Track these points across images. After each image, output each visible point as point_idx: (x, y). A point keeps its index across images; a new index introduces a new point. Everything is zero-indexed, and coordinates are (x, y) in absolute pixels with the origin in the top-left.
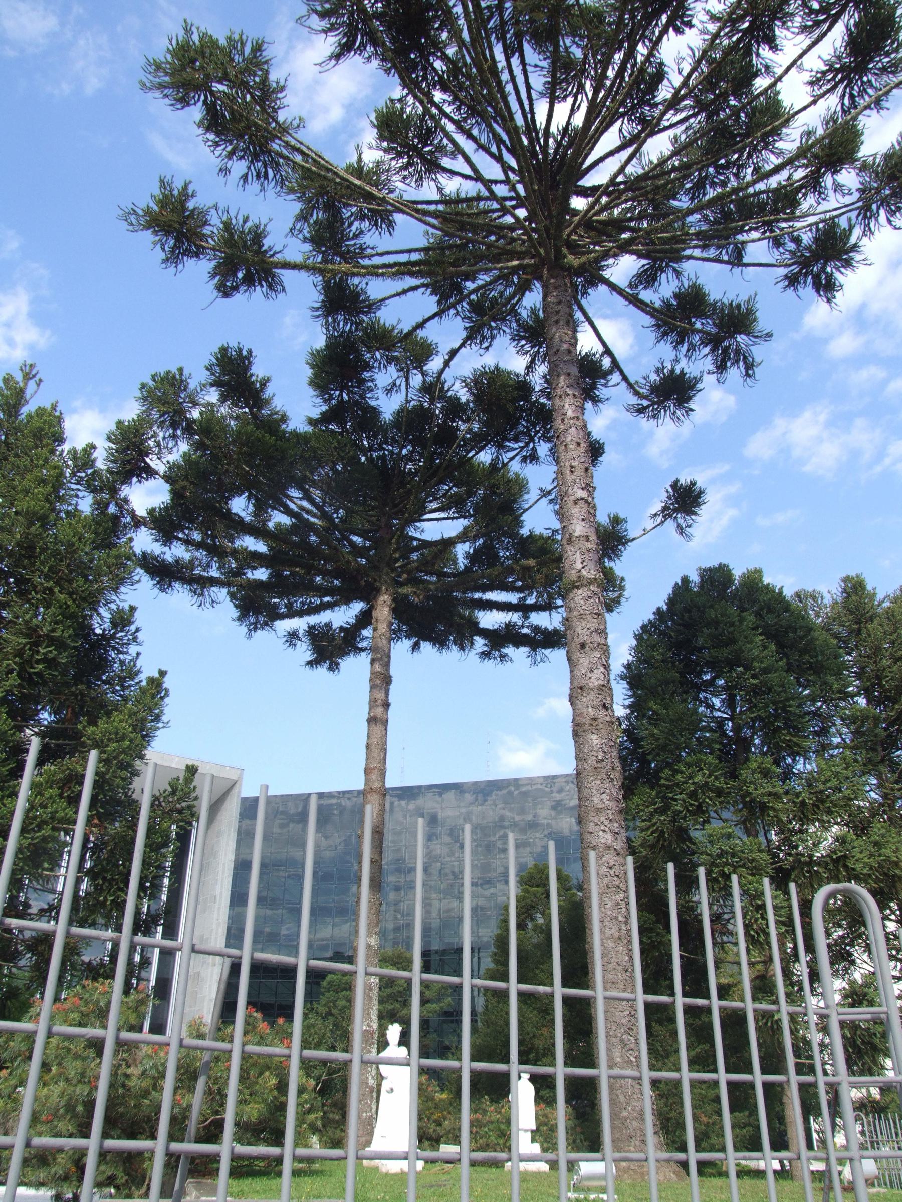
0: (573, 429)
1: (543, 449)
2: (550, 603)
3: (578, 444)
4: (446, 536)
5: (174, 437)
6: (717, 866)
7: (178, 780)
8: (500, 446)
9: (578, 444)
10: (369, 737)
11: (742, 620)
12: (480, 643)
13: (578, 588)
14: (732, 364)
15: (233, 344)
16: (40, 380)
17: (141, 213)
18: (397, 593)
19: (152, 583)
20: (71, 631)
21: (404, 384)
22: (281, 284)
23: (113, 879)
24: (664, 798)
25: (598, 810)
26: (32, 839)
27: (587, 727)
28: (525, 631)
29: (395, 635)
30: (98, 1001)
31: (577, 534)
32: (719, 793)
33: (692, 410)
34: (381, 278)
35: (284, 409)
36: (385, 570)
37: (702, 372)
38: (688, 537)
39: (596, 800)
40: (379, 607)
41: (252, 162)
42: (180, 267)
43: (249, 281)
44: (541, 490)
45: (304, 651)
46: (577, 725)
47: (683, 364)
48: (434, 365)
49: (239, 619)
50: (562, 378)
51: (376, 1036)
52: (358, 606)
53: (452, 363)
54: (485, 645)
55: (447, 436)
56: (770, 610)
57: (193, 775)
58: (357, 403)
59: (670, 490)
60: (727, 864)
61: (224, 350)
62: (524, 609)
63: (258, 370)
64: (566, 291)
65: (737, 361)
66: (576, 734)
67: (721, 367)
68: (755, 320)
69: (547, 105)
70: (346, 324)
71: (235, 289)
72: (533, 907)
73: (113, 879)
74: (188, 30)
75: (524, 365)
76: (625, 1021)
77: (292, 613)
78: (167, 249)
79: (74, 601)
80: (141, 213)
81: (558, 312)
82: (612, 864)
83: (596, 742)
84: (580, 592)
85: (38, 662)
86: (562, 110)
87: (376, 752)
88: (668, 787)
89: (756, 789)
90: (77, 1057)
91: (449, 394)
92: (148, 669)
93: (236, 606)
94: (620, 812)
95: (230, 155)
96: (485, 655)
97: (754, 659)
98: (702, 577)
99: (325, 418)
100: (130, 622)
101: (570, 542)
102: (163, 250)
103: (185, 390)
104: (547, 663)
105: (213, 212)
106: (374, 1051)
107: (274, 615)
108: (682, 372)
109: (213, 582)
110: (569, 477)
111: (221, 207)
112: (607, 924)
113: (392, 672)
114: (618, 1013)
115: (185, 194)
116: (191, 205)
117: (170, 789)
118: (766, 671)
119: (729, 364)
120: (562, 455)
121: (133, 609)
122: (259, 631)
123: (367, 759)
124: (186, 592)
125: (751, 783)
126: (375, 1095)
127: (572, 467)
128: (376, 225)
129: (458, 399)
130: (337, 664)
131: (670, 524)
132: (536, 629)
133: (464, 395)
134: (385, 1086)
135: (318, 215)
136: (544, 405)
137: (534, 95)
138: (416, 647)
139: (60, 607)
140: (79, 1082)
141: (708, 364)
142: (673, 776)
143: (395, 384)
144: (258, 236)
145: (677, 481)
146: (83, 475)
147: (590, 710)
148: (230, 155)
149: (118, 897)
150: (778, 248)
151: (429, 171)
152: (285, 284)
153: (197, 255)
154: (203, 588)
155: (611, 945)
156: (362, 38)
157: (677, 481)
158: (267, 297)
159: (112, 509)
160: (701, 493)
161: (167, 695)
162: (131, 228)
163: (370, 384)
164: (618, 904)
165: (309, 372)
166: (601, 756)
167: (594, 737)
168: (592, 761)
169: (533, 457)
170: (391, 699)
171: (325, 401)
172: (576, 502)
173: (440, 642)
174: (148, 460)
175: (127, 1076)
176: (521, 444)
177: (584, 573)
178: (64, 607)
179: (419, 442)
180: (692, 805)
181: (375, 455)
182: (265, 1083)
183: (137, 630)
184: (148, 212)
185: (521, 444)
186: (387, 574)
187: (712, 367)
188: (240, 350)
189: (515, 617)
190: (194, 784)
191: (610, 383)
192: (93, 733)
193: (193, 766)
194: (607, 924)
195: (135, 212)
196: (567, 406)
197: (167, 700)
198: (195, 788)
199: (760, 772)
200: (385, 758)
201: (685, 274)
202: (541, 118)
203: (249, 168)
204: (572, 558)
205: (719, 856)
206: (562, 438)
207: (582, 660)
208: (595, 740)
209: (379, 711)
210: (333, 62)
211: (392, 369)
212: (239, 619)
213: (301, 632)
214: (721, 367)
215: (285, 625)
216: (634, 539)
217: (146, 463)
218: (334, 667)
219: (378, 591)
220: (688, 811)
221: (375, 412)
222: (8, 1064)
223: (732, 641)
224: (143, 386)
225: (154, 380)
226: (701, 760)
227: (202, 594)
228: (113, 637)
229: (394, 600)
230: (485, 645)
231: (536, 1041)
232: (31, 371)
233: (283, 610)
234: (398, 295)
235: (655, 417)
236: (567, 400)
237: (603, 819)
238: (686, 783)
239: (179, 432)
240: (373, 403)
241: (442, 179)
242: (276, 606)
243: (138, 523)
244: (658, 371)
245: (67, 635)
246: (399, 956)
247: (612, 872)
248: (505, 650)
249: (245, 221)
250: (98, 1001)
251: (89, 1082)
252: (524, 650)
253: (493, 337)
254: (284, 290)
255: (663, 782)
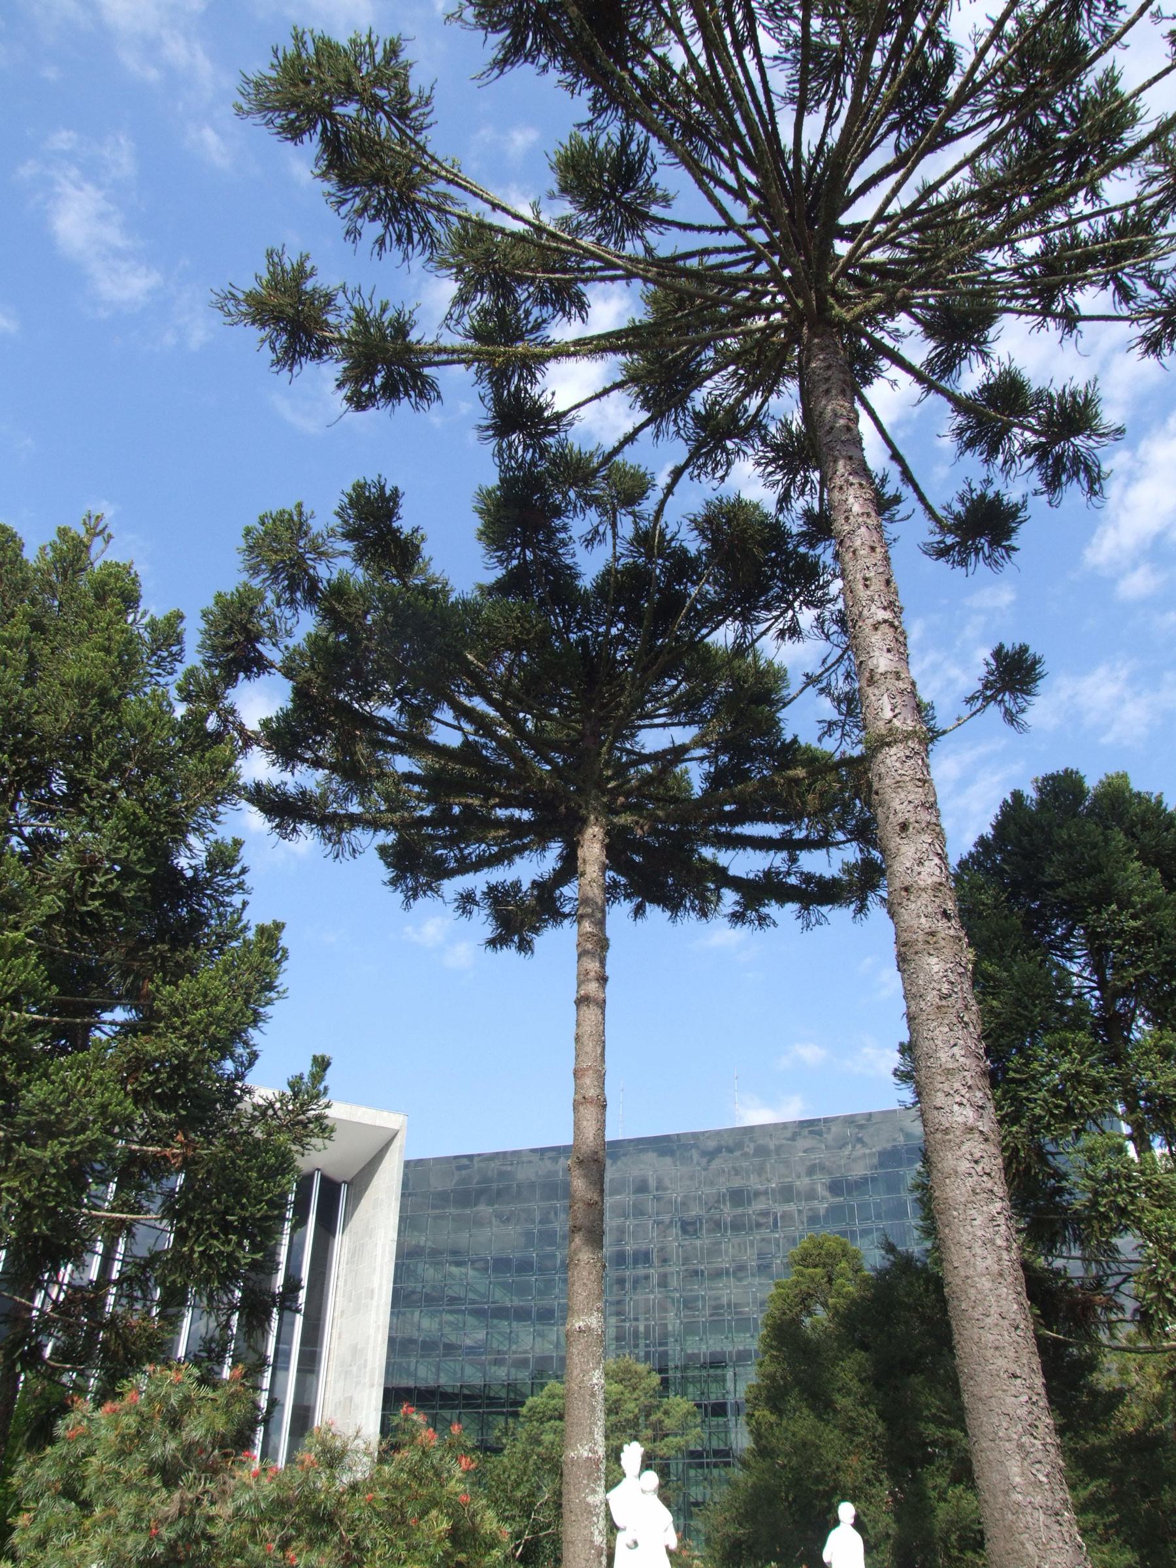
0: (863, 529)
1: (807, 617)
2: (825, 837)
3: (873, 549)
4: (678, 742)
5: (292, 602)
6: (1104, 1195)
7: (301, 1077)
8: (747, 619)
9: (873, 549)
10: (578, 1025)
11: (1107, 841)
12: (730, 898)
13: (889, 745)
14: (1069, 478)
15: (371, 478)
16: (110, 536)
17: (241, 297)
18: (611, 823)
19: (270, 825)
20: (141, 853)
21: (609, 533)
22: (433, 386)
23: (202, 1220)
24: (1015, 1099)
25: (949, 1072)
26: (72, 1145)
27: (920, 946)
28: (793, 880)
29: (611, 890)
30: (167, 1396)
31: (881, 670)
32: (1097, 1087)
33: (1014, 549)
34: (573, 359)
35: (446, 575)
36: (593, 792)
37: (1025, 496)
38: (1021, 728)
39: (943, 1056)
40: (587, 844)
41: (390, 221)
42: (296, 369)
43: (391, 391)
44: (807, 675)
45: (482, 924)
46: (905, 945)
47: (998, 485)
48: (648, 506)
49: (394, 882)
50: (841, 463)
51: (603, 1467)
52: (555, 849)
53: (675, 490)
54: (737, 903)
55: (672, 604)
56: (1146, 827)
57: (325, 1070)
58: (546, 563)
59: (992, 661)
60: (1120, 1191)
61: (360, 488)
62: (787, 844)
63: (405, 522)
64: (838, 353)
65: (1076, 474)
66: (902, 960)
67: (1053, 484)
68: (1096, 415)
69: (794, 114)
70: (525, 449)
71: (371, 397)
72: (810, 1295)
73: (202, 1220)
74: (298, 38)
75: (776, 497)
76: (1022, 1412)
77: (466, 866)
78: (278, 345)
79: (147, 811)
80: (241, 297)
81: (827, 380)
82: (977, 1155)
83: (936, 968)
84: (893, 750)
85: (94, 897)
86: (814, 123)
87: (589, 1045)
88: (1020, 1082)
89: (1155, 1077)
90: (129, 1486)
91: (673, 544)
92: (256, 916)
93: (388, 865)
94: (983, 1074)
95: (360, 213)
96: (737, 918)
97: (1131, 893)
98: (1039, 790)
99: (502, 588)
100: (234, 860)
101: (871, 681)
102: (273, 349)
103: (306, 534)
104: (825, 926)
105: (341, 296)
106: (601, 1490)
107: (440, 871)
108: (997, 494)
109: (354, 820)
110: (862, 593)
111: (351, 288)
112: (979, 1251)
113: (609, 934)
114: (1010, 1400)
115: (301, 273)
116: (309, 286)
117: (289, 1093)
118: (1150, 908)
119: (1064, 478)
120: (850, 566)
121: (238, 843)
122: (420, 900)
123: (577, 1056)
124: (317, 840)
125: (1146, 1069)
126: (604, 1560)
127: (866, 579)
128: (563, 309)
129: (685, 551)
130: (530, 943)
131: (994, 711)
132: (808, 878)
133: (693, 544)
134: (621, 1540)
135: (483, 300)
136: (805, 556)
137: (777, 104)
138: (639, 911)
139: (126, 818)
140: (133, 1528)
141: (1035, 481)
142: (1026, 1065)
143: (597, 532)
144: (401, 328)
145: (1001, 647)
146: (165, 654)
147: (923, 920)
148: (360, 213)
149: (211, 1246)
150: (1127, 303)
151: (633, 227)
152: (441, 389)
153: (319, 355)
154: (341, 830)
155: (988, 1285)
156: (535, 38)
157: (1001, 647)
158: (416, 407)
159: (212, 723)
160: (1036, 662)
161: (285, 956)
162: (229, 320)
163: (562, 535)
164: (993, 1219)
165: (477, 523)
166: (945, 988)
167: (933, 960)
168: (932, 997)
169: (793, 631)
170: (609, 971)
171: (501, 561)
172: (876, 627)
173: (673, 905)
174: (259, 646)
175: (210, 1519)
176: (775, 613)
177: (897, 723)
178: (131, 820)
179: (633, 617)
180: (1057, 1106)
181: (573, 637)
182: (431, 1528)
183: (244, 871)
184: (251, 297)
185: (775, 613)
186: (597, 798)
187: (1040, 485)
188: (382, 488)
189: (777, 860)
190: (324, 1084)
191: (897, 517)
192: (171, 995)
193: (323, 1058)
194: (979, 1251)
195: (234, 297)
196: (851, 500)
197: (285, 965)
198: (326, 1088)
199: (1158, 1053)
200: (603, 1055)
201: (994, 356)
202: (786, 138)
203: (386, 227)
204: (876, 705)
205: (1108, 1180)
206: (848, 543)
207: (904, 849)
208: (934, 965)
209: (592, 987)
210: (496, 72)
211: (593, 515)
212: (394, 882)
213: (478, 896)
214: (1053, 484)
215: (453, 886)
216: (944, 732)
217: (257, 650)
218: (525, 946)
219: (584, 822)
220: (1053, 1115)
221: (569, 574)
222: (32, 1505)
223: (1098, 869)
224: (248, 532)
225: (263, 524)
226: (1066, 1040)
227: (339, 842)
228: (209, 882)
229: (607, 833)
230: (737, 903)
231: (841, 1476)
232: (97, 525)
233: (453, 865)
234: (598, 396)
235: (963, 563)
236: (851, 491)
237: (957, 1085)
238: (1047, 1073)
239: (299, 595)
240: (569, 561)
241: (651, 235)
242: (442, 860)
243: (249, 740)
244: (962, 500)
245: (135, 858)
246: (627, 1370)
247: (979, 1168)
248: (764, 910)
249: (384, 310)
250: (167, 1396)
251: (149, 1528)
252: (792, 907)
253: (729, 464)
254: (439, 397)
255: (1012, 1074)
